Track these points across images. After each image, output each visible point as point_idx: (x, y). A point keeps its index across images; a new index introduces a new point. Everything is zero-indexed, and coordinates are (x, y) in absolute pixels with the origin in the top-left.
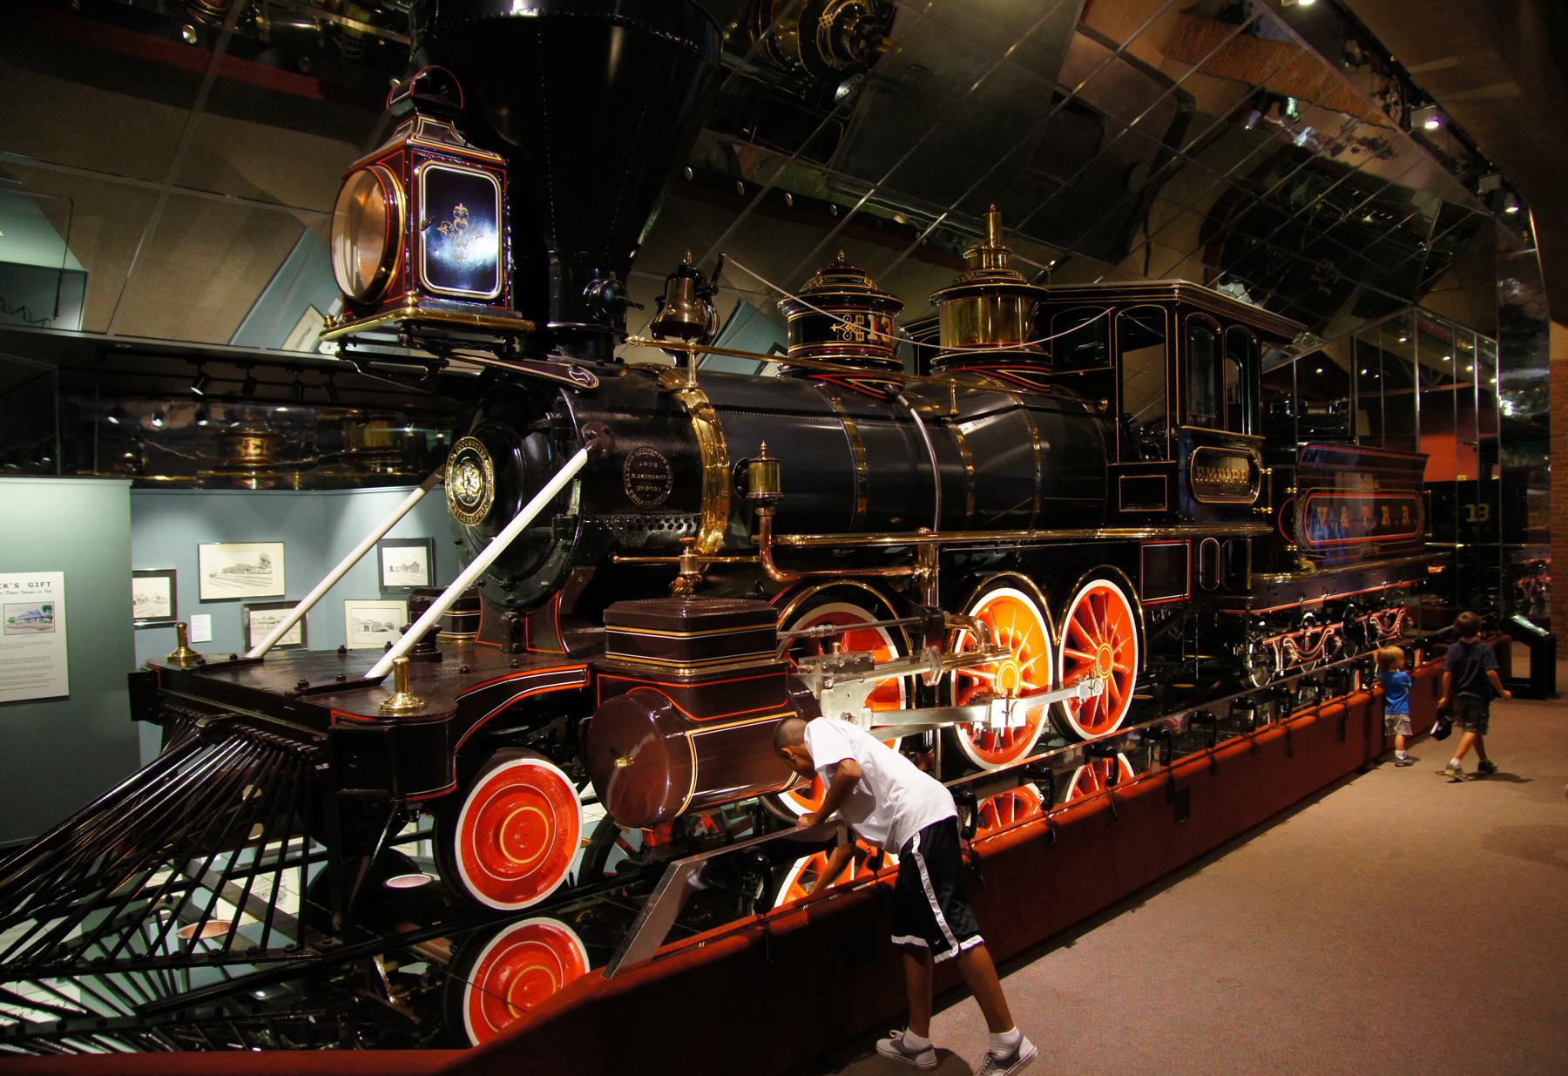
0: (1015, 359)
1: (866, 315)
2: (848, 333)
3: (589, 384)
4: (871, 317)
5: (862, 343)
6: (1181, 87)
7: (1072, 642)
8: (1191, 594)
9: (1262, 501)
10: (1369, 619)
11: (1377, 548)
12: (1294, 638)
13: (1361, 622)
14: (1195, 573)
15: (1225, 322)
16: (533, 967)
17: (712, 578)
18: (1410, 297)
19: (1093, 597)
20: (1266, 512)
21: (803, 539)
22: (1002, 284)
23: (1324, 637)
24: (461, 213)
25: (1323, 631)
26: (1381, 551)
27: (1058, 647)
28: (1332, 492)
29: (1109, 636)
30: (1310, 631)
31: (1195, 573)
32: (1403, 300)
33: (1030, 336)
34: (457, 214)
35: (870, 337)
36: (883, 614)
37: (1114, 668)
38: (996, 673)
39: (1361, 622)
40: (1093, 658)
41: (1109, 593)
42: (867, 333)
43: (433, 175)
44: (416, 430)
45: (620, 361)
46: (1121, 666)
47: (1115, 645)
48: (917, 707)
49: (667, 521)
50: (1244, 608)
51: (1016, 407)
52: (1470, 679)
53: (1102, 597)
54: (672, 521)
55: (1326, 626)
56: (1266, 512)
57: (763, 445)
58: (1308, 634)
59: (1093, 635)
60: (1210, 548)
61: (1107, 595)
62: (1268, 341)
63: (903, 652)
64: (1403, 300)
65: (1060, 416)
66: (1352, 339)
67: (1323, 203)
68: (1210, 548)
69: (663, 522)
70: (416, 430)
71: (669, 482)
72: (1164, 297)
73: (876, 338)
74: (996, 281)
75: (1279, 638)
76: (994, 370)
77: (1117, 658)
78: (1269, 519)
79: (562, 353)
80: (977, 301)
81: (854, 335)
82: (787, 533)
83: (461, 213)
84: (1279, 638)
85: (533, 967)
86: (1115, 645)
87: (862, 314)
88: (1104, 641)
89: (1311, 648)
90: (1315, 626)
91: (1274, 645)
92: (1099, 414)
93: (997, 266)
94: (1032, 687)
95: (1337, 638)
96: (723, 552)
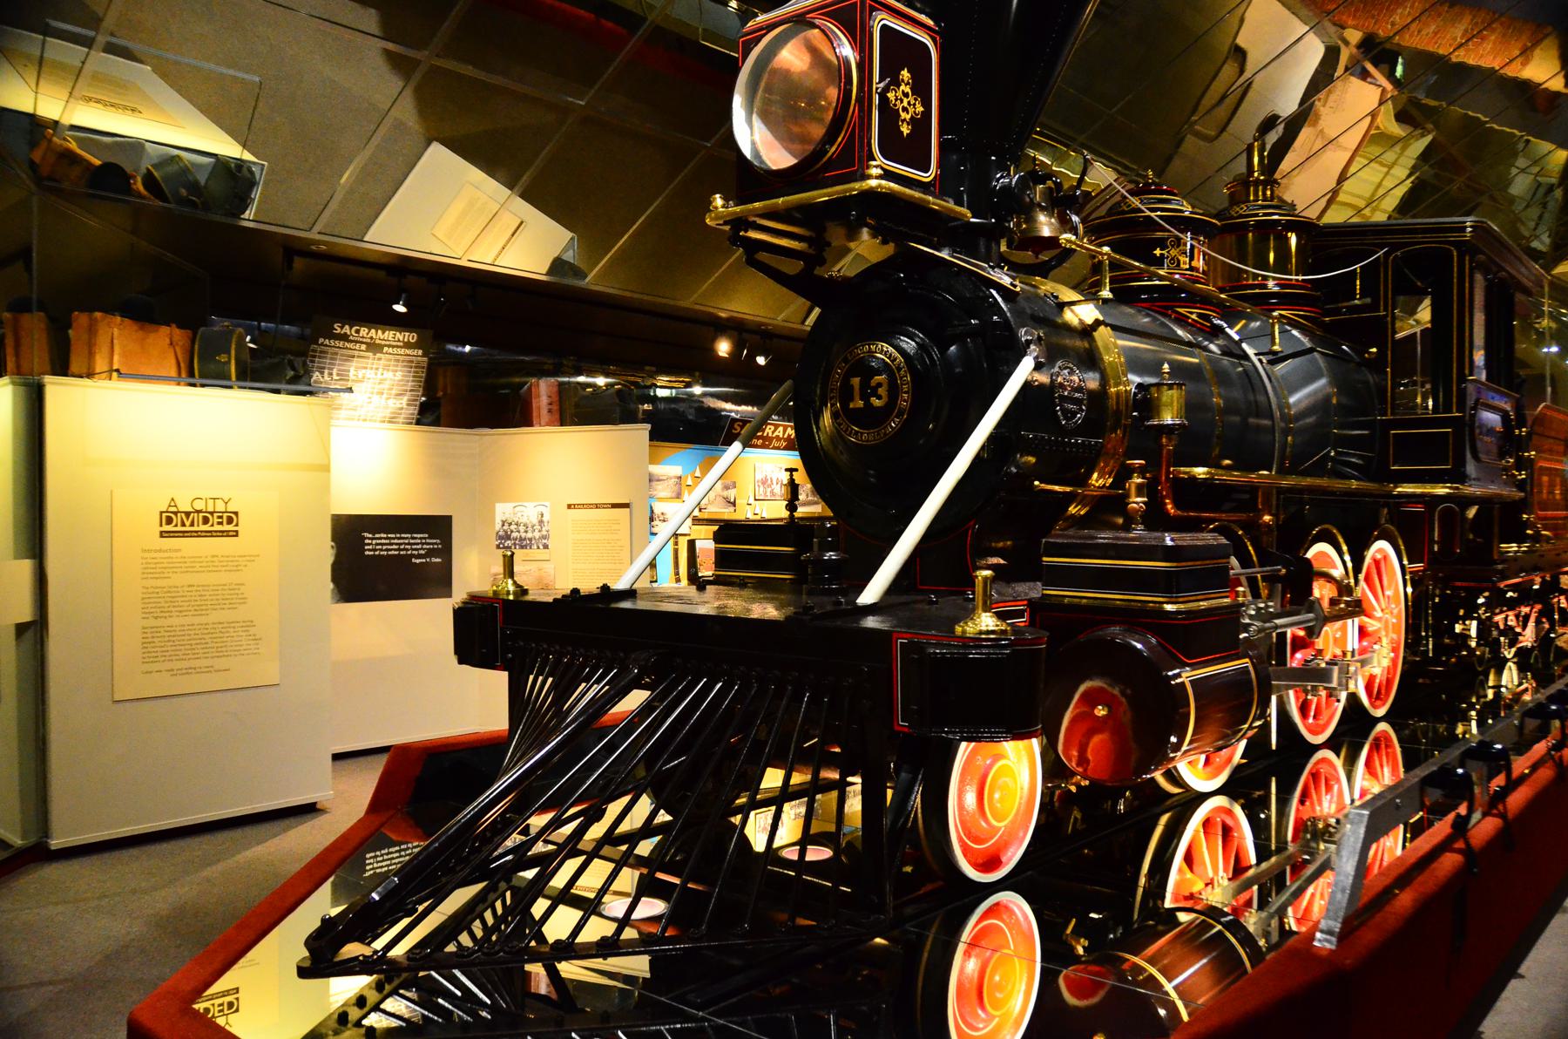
5: (1186, 270)
59: (1377, 599)
81: (1179, 261)
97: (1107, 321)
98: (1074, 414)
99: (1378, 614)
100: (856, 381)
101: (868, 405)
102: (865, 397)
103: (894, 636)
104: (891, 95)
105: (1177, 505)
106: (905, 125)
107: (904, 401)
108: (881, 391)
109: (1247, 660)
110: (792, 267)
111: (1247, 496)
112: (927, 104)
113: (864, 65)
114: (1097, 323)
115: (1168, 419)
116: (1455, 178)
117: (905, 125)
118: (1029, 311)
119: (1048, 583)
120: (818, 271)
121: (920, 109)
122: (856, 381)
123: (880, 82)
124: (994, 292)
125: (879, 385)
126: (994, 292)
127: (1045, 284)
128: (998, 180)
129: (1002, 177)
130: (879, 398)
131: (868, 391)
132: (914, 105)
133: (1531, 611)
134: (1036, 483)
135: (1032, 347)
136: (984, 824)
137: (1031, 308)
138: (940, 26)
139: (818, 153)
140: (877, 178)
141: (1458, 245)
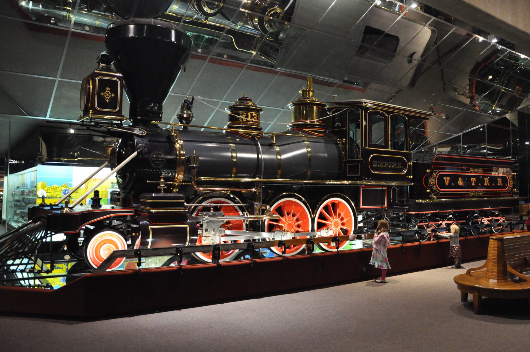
6: (387, 33)
7: (321, 217)
9: (408, 174)
15: (389, 113)
20: (410, 178)
21: (204, 178)
24: (108, 89)
34: (107, 90)
38: (295, 226)
40: (331, 223)
43: (100, 80)
44: (412, 166)
47: (342, 219)
48: (72, 181)
49: (164, 172)
52: (309, 208)
53: (337, 204)
54: (166, 172)
56: (410, 178)
61: (339, 203)
69: (163, 172)
70: (412, 166)
76: (302, 129)
77: (343, 224)
78: (412, 180)
80: (301, 107)
81: (243, 119)
82: (201, 177)
83: (108, 89)
91: (424, 226)
93: (309, 96)
94: (300, 230)
96: (183, 182)
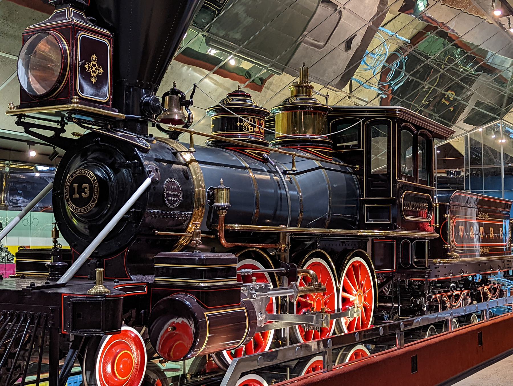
0: (315, 143)
1: (254, 118)
2: (245, 127)
3: (147, 147)
4: (256, 120)
5: (252, 132)
8: (396, 268)
10: (483, 289)
11: (488, 250)
12: (448, 296)
13: (479, 291)
14: (398, 257)
16: (124, 352)
17: (113, 159)
18: (498, 115)
19: (353, 265)
22: (310, 104)
23: (462, 297)
25: (461, 293)
26: (490, 251)
27: (339, 290)
28: (466, 218)
29: (361, 287)
30: (455, 293)
31: (398, 257)
32: (496, 116)
33: (322, 132)
35: (255, 130)
36: (267, 265)
37: (364, 304)
39: (479, 291)
41: (361, 264)
42: (254, 127)
45: (151, 135)
46: (367, 304)
50: (424, 277)
51: (319, 168)
55: (462, 291)
57: (222, 180)
58: (454, 294)
59: (354, 285)
60: (406, 244)
62: (437, 138)
63: (275, 285)
64: (496, 116)
65: (342, 174)
66: (466, 138)
67: (441, 68)
68: (406, 244)
71: (181, 196)
72: (391, 115)
73: (258, 130)
74: (306, 103)
75: (440, 295)
76: (305, 148)
79: (257, 123)
81: (248, 128)
84: (440, 295)
85: (124, 352)
86: (364, 292)
87: (252, 118)
88: (359, 289)
89: (455, 302)
90: (457, 291)
92: (355, 173)
95: (468, 298)
97: (197, 160)
98: (175, 202)
99: (355, 292)
100: (76, 186)
101: (81, 196)
102: (79, 193)
103: (63, 295)
104: (86, 66)
105: (227, 241)
106: (93, 78)
107: (96, 195)
108: (86, 190)
109: (244, 308)
110: (50, 134)
111: (276, 236)
112: (105, 69)
113: (73, 55)
114: (192, 161)
115: (222, 203)
116: (422, 82)
117: (93, 78)
118: (154, 157)
119: (157, 276)
120: (62, 135)
121: (101, 71)
122: (76, 186)
123: (80, 61)
124: (136, 149)
125: (86, 188)
126: (136, 149)
127: (173, 143)
128: (144, 99)
129: (146, 97)
130: (85, 193)
131: (81, 191)
132: (98, 69)
133: (461, 293)
134: (156, 231)
135: (152, 173)
136: (116, 379)
137: (156, 155)
138: (113, 35)
139: (54, 89)
140: (76, 103)
141: (393, 118)
